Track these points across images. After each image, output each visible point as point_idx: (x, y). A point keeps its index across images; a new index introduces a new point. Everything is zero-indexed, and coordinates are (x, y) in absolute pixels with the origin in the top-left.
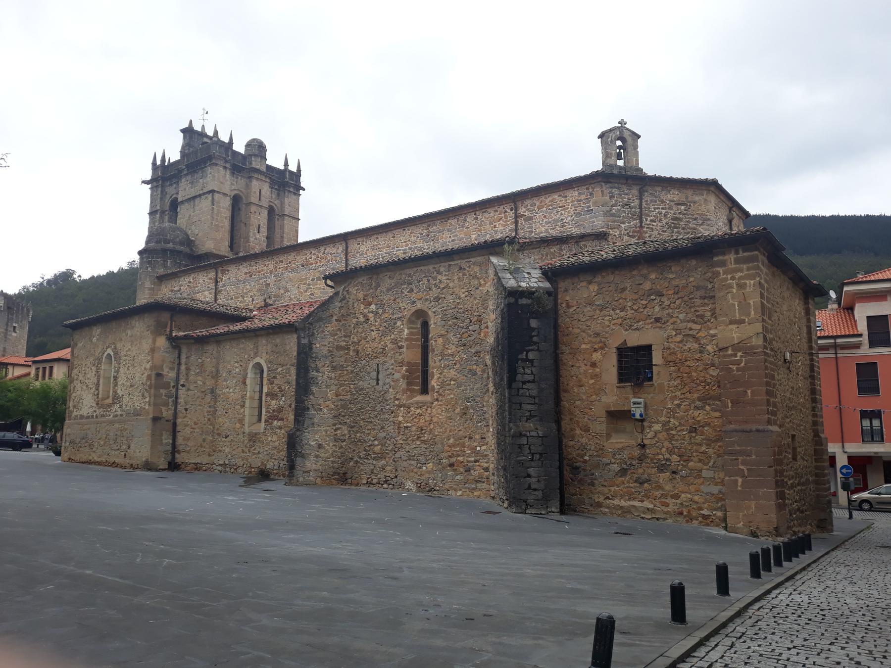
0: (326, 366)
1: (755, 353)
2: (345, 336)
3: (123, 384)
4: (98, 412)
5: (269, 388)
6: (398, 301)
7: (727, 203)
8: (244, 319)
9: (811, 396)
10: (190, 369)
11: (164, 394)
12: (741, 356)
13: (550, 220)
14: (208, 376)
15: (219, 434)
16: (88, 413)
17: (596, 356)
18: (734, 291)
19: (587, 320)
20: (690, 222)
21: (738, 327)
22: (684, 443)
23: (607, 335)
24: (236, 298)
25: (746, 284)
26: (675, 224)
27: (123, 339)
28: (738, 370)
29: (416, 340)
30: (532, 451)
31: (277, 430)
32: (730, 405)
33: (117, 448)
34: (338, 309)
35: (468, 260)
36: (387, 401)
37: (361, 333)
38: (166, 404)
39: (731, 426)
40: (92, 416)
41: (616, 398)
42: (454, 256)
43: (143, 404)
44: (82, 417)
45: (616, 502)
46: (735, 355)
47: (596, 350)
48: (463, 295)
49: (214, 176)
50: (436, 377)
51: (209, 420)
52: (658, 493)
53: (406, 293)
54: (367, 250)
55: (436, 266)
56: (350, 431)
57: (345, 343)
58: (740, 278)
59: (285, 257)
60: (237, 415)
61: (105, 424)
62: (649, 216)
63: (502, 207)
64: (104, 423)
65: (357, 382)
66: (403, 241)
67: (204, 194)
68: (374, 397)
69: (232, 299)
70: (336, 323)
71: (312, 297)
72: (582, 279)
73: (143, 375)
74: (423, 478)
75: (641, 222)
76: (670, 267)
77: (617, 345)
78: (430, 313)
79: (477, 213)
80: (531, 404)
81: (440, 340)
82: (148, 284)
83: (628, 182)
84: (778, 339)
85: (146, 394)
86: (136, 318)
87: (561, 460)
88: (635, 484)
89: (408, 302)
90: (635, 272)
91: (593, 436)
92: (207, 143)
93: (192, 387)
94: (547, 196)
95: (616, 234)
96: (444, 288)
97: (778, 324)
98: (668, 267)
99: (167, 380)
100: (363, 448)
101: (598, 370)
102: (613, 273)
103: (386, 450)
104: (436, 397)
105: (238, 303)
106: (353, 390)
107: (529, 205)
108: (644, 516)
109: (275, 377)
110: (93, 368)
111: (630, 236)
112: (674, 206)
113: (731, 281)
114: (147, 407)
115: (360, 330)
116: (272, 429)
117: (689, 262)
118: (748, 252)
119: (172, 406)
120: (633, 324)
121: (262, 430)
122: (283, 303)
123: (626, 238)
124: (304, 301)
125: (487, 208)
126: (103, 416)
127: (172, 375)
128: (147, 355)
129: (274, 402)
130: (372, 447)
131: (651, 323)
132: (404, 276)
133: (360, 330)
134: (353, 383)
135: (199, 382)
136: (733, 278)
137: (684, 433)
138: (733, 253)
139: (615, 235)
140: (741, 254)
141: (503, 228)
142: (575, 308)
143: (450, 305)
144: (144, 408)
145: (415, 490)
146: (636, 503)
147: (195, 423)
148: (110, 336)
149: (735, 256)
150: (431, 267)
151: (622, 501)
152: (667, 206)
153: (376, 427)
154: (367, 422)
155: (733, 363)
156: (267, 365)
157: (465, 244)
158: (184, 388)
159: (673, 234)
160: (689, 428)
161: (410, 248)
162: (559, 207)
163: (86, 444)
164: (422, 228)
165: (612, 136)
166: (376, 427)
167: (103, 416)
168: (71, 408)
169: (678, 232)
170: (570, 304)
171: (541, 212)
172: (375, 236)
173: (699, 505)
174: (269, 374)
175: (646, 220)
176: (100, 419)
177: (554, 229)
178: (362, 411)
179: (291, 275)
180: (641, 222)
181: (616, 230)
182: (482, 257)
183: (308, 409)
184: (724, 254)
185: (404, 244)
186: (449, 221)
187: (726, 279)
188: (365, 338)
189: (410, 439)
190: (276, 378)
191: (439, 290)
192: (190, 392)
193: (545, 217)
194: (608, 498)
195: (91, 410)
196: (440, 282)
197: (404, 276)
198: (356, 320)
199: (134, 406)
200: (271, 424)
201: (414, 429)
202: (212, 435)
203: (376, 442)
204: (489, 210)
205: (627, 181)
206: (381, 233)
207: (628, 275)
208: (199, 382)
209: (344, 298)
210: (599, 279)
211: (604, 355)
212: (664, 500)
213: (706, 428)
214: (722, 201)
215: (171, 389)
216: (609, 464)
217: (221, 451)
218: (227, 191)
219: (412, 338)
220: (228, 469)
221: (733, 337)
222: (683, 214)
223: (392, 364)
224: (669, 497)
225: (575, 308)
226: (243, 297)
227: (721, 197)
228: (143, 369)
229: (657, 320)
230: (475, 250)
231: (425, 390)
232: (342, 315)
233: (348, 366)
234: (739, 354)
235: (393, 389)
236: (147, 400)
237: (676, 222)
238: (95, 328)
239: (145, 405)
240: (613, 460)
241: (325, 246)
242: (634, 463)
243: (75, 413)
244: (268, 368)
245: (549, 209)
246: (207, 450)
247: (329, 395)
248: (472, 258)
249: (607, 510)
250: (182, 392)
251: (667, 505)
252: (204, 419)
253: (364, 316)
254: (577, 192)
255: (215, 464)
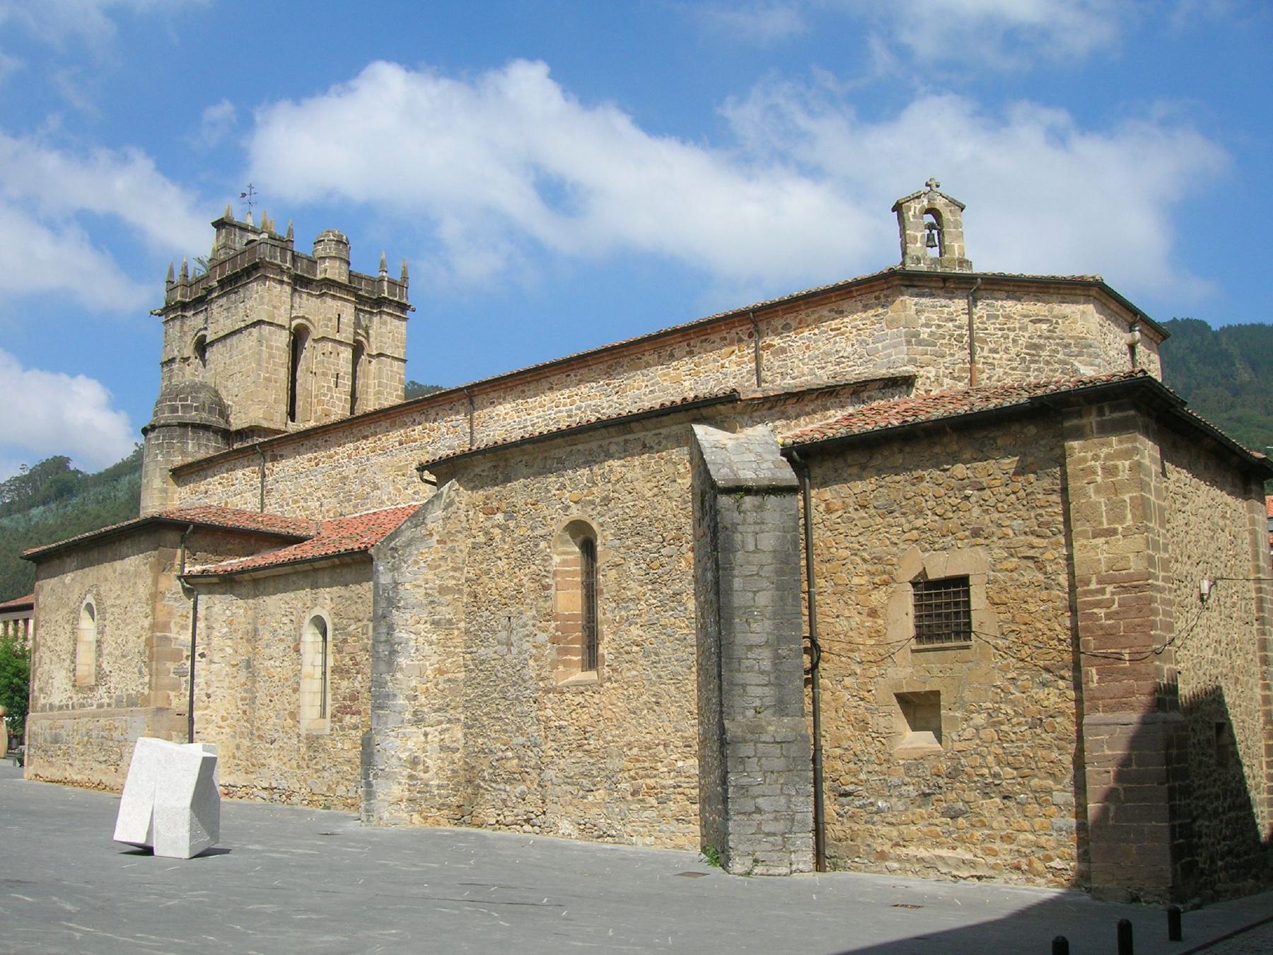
0: (422, 622)
1: (1135, 587)
2: (455, 569)
3: (111, 653)
4: (75, 699)
5: (336, 660)
6: (540, 505)
7: (1124, 315)
8: (299, 540)
9: (1258, 654)
10: (213, 628)
11: (172, 671)
12: (1113, 594)
13: (817, 352)
14: (241, 638)
15: (260, 737)
16: (61, 701)
17: (877, 597)
18: (1099, 479)
19: (860, 534)
20: (1058, 352)
21: (1107, 542)
22: (1022, 747)
23: (895, 560)
24: (296, 502)
25: (1116, 467)
26: (1033, 355)
27: (109, 578)
28: (1108, 616)
29: (573, 574)
30: (765, 768)
31: (351, 731)
32: (1096, 678)
33: (104, 759)
34: (441, 521)
35: (657, 431)
36: (525, 681)
37: (482, 563)
38: (176, 687)
39: (1098, 714)
40: (67, 706)
41: (910, 670)
42: (632, 425)
43: (141, 687)
44: (52, 707)
45: (912, 850)
46: (1102, 591)
47: (876, 586)
48: (650, 494)
49: (262, 297)
50: (606, 639)
51: (245, 712)
52: (978, 834)
53: (554, 492)
54: (506, 414)
55: (604, 443)
56: (465, 735)
57: (454, 582)
58: (1108, 457)
59: (372, 430)
60: (287, 705)
61: (86, 719)
62: (985, 342)
63: (733, 331)
64: (85, 717)
65: (474, 649)
66: (566, 396)
67: (247, 327)
68: (505, 675)
69: (288, 505)
70: (439, 546)
71: (416, 497)
72: (849, 460)
73: (139, 637)
74: (588, 816)
75: (972, 354)
76: (994, 439)
77: (911, 578)
78: (595, 525)
79: (692, 342)
80: (763, 685)
81: (613, 574)
82: (157, 483)
83: (947, 285)
84: (1185, 559)
85: (145, 670)
86: (128, 542)
87: (817, 782)
88: (943, 819)
89: (558, 506)
90: (937, 450)
91: (873, 738)
92: (254, 241)
93: (216, 659)
94: (809, 311)
95: (929, 375)
96: (618, 481)
97: (1187, 532)
98: (992, 438)
99: (176, 647)
100: (486, 762)
101: (880, 622)
102: (901, 451)
103: (526, 766)
104: (607, 675)
105: (298, 511)
106: (470, 663)
107: (780, 327)
108: (956, 873)
109: (345, 641)
110: (66, 626)
111: (954, 378)
112: (1030, 324)
113: (1093, 463)
114: (146, 691)
115: (479, 558)
116: (342, 728)
117: (1025, 431)
118: (1119, 411)
119: (186, 690)
120: (936, 540)
121: (328, 731)
122: (369, 509)
123: (947, 381)
124: (403, 506)
125: (709, 334)
126: (82, 706)
127: (187, 637)
128: (145, 605)
129: (345, 683)
130: (504, 761)
131: (967, 537)
132: (549, 462)
133: (479, 558)
134: (469, 650)
135: (227, 649)
136: (1096, 458)
137: (1023, 729)
138: (1094, 413)
139: (928, 378)
140: (1108, 416)
141: (737, 368)
142: (840, 513)
143: (627, 510)
144: (143, 693)
145: (576, 833)
146: (944, 852)
147: (224, 719)
148: (91, 574)
149: (1099, 419)
150: (594, 445)
151: (921, 849)
152: (1017, 325)
153: (509, 728)
154: (494, 718)
155: (1098, 604)
156: (332, 619)
157: (672, 399)
158: (204, 659)
159: (1030, 374)
160: (1030, 720)
161: (579, 408)
162: (831, 330)
163: (59, 752)
164: (598, 372)
165: (915, 208)
166: (509, 728)
167: (82, 706)
168: (36, 694)
169: (1038, 370)
170: (831, 506)
171: (800, 339)
172: (520, 388)
173: (1046, 852)
174: (336, 635)
175: (982, 349)
176: (78, 712)
177: (823, 368)
178: (485, 698)
179: (382, 460)
180: (972, 354)
181: (930, 368)
182: (680, 426)
183: (395, 695)
184: (1080, 415)
185: (568, 401)
186: (645, 358)
187: (1084, 460)
188: (487, 572)
189: (566, 747)
190: (347, 642)
191: (610, 485)
192: (213, 666)
193: (807, 348)
194: (897, 844)
195: (65, 696)
196: (611, 471)
197: (549, 462)
198: (473, 540)
199: (127, 690)
200: (341, 721)
201: (572, 729)
202: (250, 739)
203: (510, 754)
204: (712, 337)
205: (945, 284)
206: (529, 382)
207: (926, 454)
208: (227, 649)
209: (451, 504)
210: (879, 462)
211: (890, 596)
212: (989, 845)
213: (1058, 720)
214: (1117, 313)
215: (184, 661)
216: (900, 786)
217: (264, 765)
218: (283, 320)
219: (567, 571)
220: (276, 797)
221: (1099, 560)
222: (1048, 338)
223: (534, 617)
224: (998, 841)
225: (840, 513)
226: (306, 500)
227: (1112, 306)
228: (139, 627)
229: (976, 533)
230: (668, 414)
231: (591, 660)
232: (449, 532)
233: (460, 621)
234: (1109, 589)
235: (536, 661)
236: (147, 679)
237: (1034, 352)
238: (68, 560)
239: (143, 688)
240: (907, 779)
241: (437, 409)
242: (941, 782)
243: (42, 701)
244: (335, 624)
245: (815, 334)
246: (244, 763)
247: (429, 672)
248: (663, 427)
249: (896, 865)
250: (200, 665)
251: (994, 853)
252: (235, 711)
253: (487, 533)
254: (859, 303)
255: (256, 787)
